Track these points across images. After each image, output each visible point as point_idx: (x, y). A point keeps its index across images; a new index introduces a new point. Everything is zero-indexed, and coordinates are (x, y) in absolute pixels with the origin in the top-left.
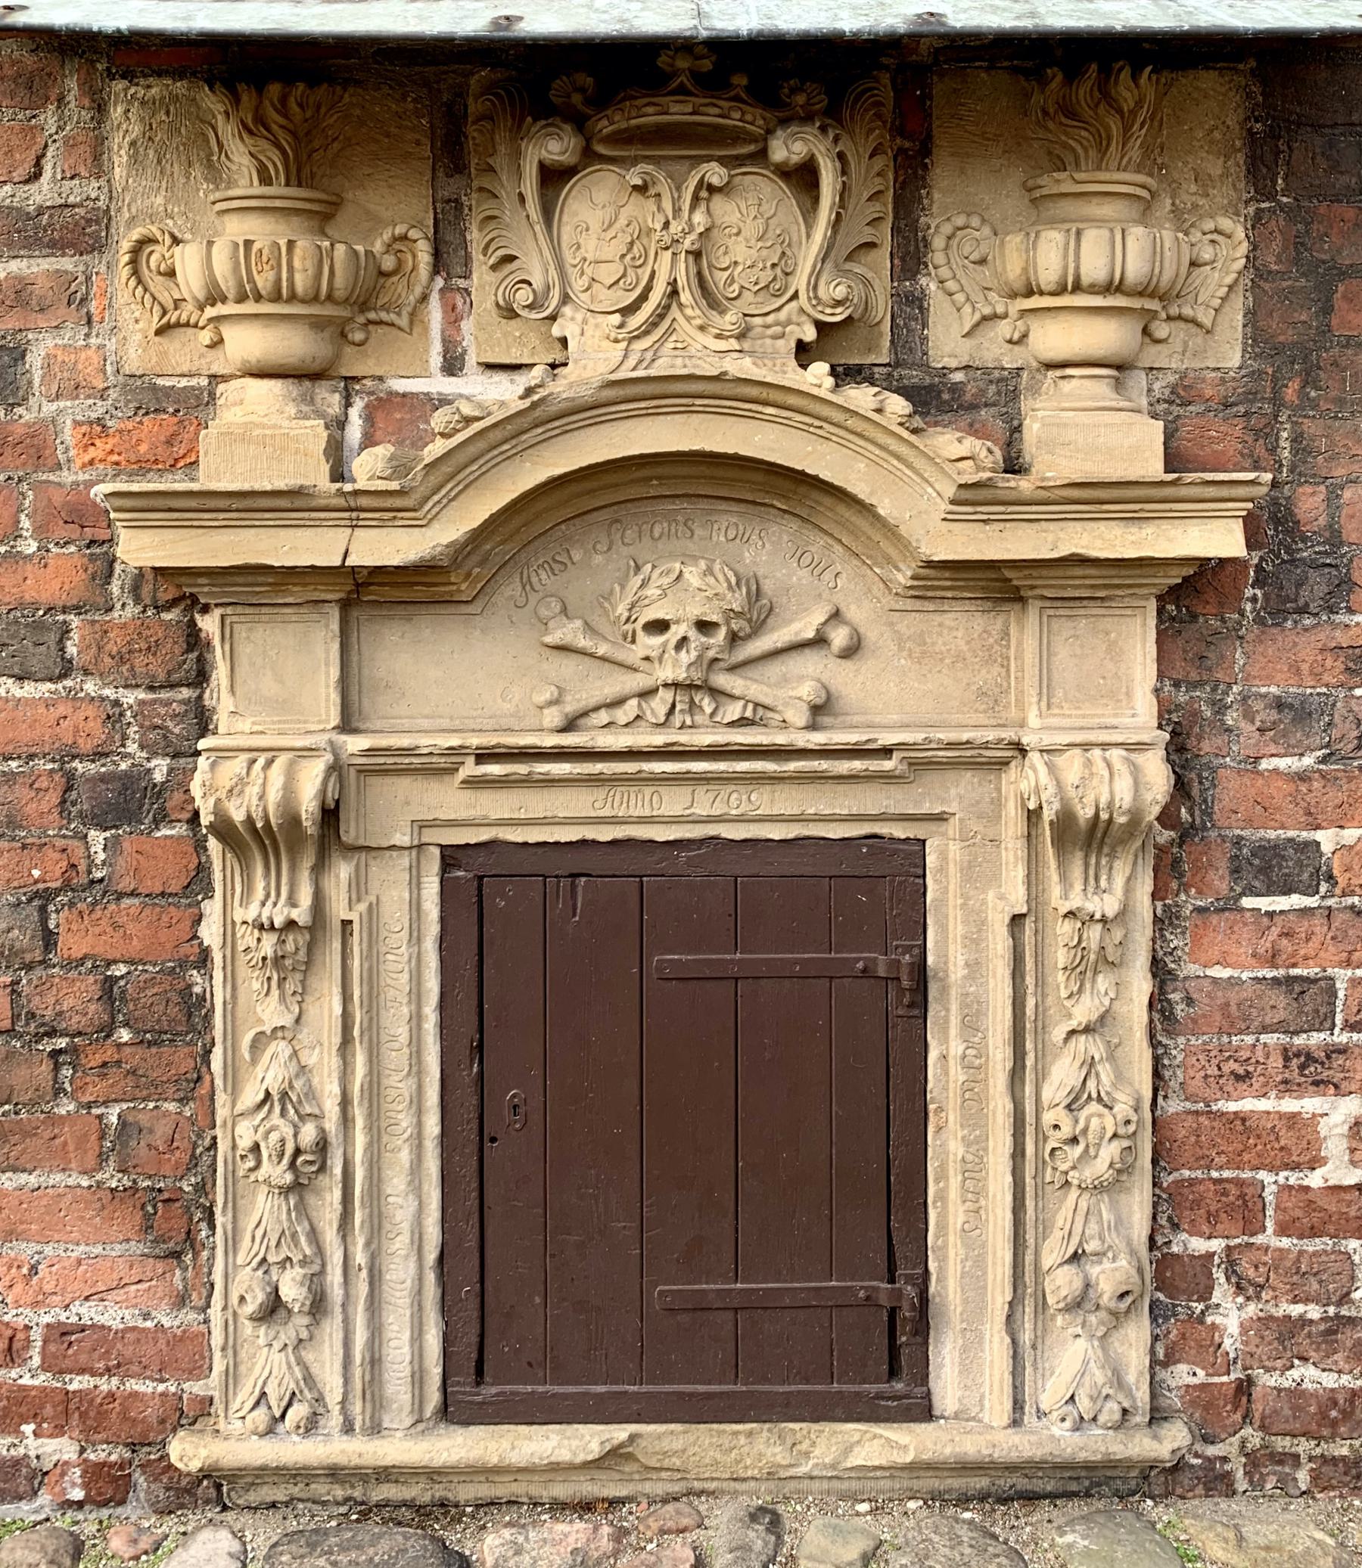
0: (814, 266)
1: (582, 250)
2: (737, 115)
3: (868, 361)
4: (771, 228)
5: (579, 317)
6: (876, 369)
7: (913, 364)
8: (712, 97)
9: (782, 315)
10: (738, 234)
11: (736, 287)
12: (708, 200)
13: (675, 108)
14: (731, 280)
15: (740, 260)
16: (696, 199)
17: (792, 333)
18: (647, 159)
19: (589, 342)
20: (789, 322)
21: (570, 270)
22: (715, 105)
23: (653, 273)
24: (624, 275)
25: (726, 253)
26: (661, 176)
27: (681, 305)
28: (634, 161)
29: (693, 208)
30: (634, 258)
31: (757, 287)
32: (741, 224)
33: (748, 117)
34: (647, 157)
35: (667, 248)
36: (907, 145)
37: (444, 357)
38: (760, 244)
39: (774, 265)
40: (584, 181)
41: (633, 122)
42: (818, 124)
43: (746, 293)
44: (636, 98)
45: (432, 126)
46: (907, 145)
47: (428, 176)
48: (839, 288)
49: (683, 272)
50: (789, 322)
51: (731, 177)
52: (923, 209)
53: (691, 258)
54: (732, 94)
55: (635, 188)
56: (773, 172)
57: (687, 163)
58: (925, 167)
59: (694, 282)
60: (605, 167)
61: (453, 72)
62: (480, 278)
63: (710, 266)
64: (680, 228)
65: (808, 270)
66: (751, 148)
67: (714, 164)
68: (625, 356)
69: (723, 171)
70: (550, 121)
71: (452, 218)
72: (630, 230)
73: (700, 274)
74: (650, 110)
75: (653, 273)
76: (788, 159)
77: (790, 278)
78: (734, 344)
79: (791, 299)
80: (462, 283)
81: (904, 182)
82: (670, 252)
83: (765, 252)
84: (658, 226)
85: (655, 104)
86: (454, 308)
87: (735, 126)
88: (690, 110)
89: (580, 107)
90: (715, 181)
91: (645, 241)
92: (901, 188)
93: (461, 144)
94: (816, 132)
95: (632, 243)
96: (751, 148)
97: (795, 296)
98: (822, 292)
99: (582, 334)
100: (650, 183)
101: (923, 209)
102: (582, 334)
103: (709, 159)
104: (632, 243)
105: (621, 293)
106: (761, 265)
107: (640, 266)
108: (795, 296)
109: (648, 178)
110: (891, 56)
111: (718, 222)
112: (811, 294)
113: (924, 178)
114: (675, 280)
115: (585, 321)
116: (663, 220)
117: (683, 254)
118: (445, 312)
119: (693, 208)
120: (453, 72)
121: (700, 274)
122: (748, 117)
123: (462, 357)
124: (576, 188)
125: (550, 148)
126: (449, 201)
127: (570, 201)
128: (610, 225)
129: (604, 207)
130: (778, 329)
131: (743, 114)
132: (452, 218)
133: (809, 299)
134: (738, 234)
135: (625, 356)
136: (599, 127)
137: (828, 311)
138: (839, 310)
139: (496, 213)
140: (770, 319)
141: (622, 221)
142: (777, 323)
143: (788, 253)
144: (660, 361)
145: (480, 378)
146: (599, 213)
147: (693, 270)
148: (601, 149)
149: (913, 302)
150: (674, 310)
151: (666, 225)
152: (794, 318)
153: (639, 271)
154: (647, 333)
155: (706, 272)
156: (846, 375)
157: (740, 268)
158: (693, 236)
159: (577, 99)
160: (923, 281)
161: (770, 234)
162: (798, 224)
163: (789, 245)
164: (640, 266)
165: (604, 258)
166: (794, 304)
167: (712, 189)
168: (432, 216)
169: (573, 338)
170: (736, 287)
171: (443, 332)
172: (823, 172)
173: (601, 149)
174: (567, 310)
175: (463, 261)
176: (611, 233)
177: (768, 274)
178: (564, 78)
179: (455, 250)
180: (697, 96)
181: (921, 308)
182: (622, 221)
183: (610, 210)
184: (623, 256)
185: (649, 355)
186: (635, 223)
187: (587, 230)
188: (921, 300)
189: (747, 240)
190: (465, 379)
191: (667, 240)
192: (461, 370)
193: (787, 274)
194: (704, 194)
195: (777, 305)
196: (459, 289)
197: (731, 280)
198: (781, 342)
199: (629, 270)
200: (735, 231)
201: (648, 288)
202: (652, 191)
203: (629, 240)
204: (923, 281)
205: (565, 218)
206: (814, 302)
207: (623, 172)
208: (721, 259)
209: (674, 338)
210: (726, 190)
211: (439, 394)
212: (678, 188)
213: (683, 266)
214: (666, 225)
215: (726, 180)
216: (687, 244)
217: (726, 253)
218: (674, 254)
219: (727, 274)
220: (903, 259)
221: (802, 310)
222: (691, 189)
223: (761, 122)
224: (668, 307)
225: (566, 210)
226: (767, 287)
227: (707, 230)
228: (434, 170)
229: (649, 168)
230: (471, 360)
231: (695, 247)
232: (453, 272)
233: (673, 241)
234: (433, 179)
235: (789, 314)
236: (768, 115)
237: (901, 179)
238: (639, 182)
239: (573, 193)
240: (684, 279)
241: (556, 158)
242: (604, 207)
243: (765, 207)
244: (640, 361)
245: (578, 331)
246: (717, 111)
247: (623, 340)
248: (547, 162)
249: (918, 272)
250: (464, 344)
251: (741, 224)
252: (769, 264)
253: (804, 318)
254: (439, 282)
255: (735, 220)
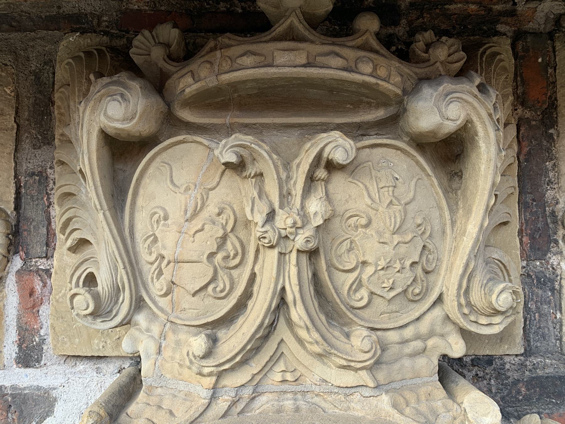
0: (467, 266)
1: (159, 244)
2: (367, 68)
3: (501, 352)
4: (410, 215)
5: (156, 329)
6: (507, 359)
7: (547, 351)
8: (333, 44)
9: (424, 326)
10: (367, 226)
11: (364, 293)
12: (327, 181)
13: (282, 58)
14: (358, 284)
15: (370, 259)
16: (311, 179)
17: (435, 347)
18: (246, 128)
19: (168, 365)
20: (432, 334)
21: (146, 268)
22: (338, 55)
23: (253, 278)
24: (214, 279)
25: (350, 250)
26: (262, 150)
27: (290, 323)
28: (230, 130)
29: (307, 191)
30: (226, 258)
31: (392, 294)
32: (372, 213)
33: (382, 72)
34: (246, 126)
35: (272, 247)
36: (528, 114)
37: (20, 346)
38: (397, 239)
39: (414, 264)
40: (164, 155)
41: (226, 77)
42: (478, 81)
43: (377, 301)
44: (229, 46)
45: (17, 96)
46: (528, 114)
47: (11, 146)
48: (504, 296)
49: (294, 280)
50: (432, 334)
51: (358, 149)
52: (550, 182)
53: (304, 259)
54: (359, 41)
55: (227, 165)
56: (408, 144)
57: (296, 133)
58: (550, 138)
59: (309, 290)
60: (189, 137)
61: (42, 38)
62: (60, 260)
63: (330, 266)
64: (290, 222)
65: (458, 269)
66: (380, 114)
67: (336, 134)
68: (213, 397)
69: (348, 143)
70: (115, 78)
71: (34, 192)
72: (222, 219)
73: (315, 276)
74: (248, 60)
75: (253, 278)
76: (440, 126)
77: (432, 277)
78: (365, 377)
79: (435, 304)
80: (42, 264)
81: (529, 153)
82: (276, 252)
83: (403, 249)
84: (259, 218)
85: (254, 54)
86: (32, 293)
87: (364, 85)
88: (304, 61)
89: (162, 64)
90: (339, 157)
91: (242, 234)
92: (527, 160)
93: (50, 114)
94: (476, 91)
95: (224, 238)
96: (380, 114)
97: (440, 300)
98: (476, 296)
99: (159, 352)
100: (248, 160)
101: (550, 182)
102: (159, 352)
103: (326, 128)
104: (224, 238)
105: (209, 301)
106: (398, 266)
107: (236, 267)
108: (440, 300)
109: (245, 153)
110: (506, 24)
111: (340, 209)
112: (463, 301)
113: (549, 150)
114: (283, 289)
115: (163, 336)
116: (266, 210)
117: (294, 255)
118: (21, 296)
119: (307, 191)
120: (42, 38)
121: (315, 276)
122: (382, 72)
123: (39, 348)
124: (154, 164)
125: (110, 112)
126: (33, 174)
127: (146, 180)
128: (195, 214)
129: (187, 189)
130: (417, 345)
131: (375, 68)
132: (34, 192)
133: (460, 305)
134: (367, 226)
135: (213, 397)
136: (181, 86)
137: (483, 320)
138: (497, 319)
139: (72, 190)
140: (408, 332)
141: (211, 209)
142: (417, 337)
143: (430, 246)
144: (263, 399)
145: (62, 368)
146: (181, 199)
147: (307, 274)
148: (186, 115)
149: (545, 284)
150: (282, 331)
151: (271, 216)
152: (438, 329)
153: (235, 273)
154: (244, 362)
155: (324, 276)
156: (473, 365)
157: (370, 270)
158: (308, 232)
159: (158, 53)
160: (554, 260)
161: (409, 224)
162: (440, 208)
163: (430, 236)
164: (236, 267)
165: (186, 258)
166: (437, 312)
167: (331, 166)
168: (13, 191)
169: (148, 356)
170: (364, 293)
171: (19, 318)
172: (482, 145)
173: (186, 115)
174: (141, 318)
175: (44, 239)
176: (197, 224)
177: (408, 275)
178: (146, 33)
179: (36, 228)
180: (312, 42)
181: (553, 290)
182: (211, 209)
183: (196, 194)
184: (212, 255)
185: (247, 393)
186: (229, 211)
187: (166, 218)
188: (552, 281)
189: (380, 234)
190: (44, 370)
191: (272, 236)
192: (38, 361)
193: (427, 272)
194: (321, 173)
195: (417, 314)
196: (38, 271)
197: (358, 284)
198: (421, 361)
199: (221, 273)
200: (363, 221)
201: (247, 295)
202: (251, 170)
203: (220, 233)
204: (554, 260)
205: (140, 201)
206: (466, 311)
207: (213, 145)
208: (345, 258)
209: (281, 366)
210: (352, 168)
211: (13, 387)
212: (287, 166)
213: (294, 271)
214: (271, 216)
215: (352, 155)
216: (300, 241)
217: (350, 250)
218: (280, 253)
219: (352, 277)
220: (532, 237)
221: (447, 318)
222: (305, 167)
223: (398, 79)
224: (272, 326)
225: (141, 192)
226: (405, 291)
227: (327, 221)
228: (18, 141)
229: (247, 139)
230: (48, 348)
231: (311, 246)
232: (32, 252)
233: (280, 237)
234: (16, 150)
235: (432, 325)
236: (407, 70)
237: (525, 150)
238: (232, 158)
239: (151, 170)
240: (296, 289)
241: (118, 125)
242: (187, 189)
243: (401, 189)
244: (234, 403)
245: (152, 347)
246: (339, 62)
247: (210, 374)
248: (110, 131)
249: (548, 250)
250: (42, 332)
251: (372, 213)
252: (408, 263)
253: (449, 328)
254: (17, 263)
255: (363, 207)
